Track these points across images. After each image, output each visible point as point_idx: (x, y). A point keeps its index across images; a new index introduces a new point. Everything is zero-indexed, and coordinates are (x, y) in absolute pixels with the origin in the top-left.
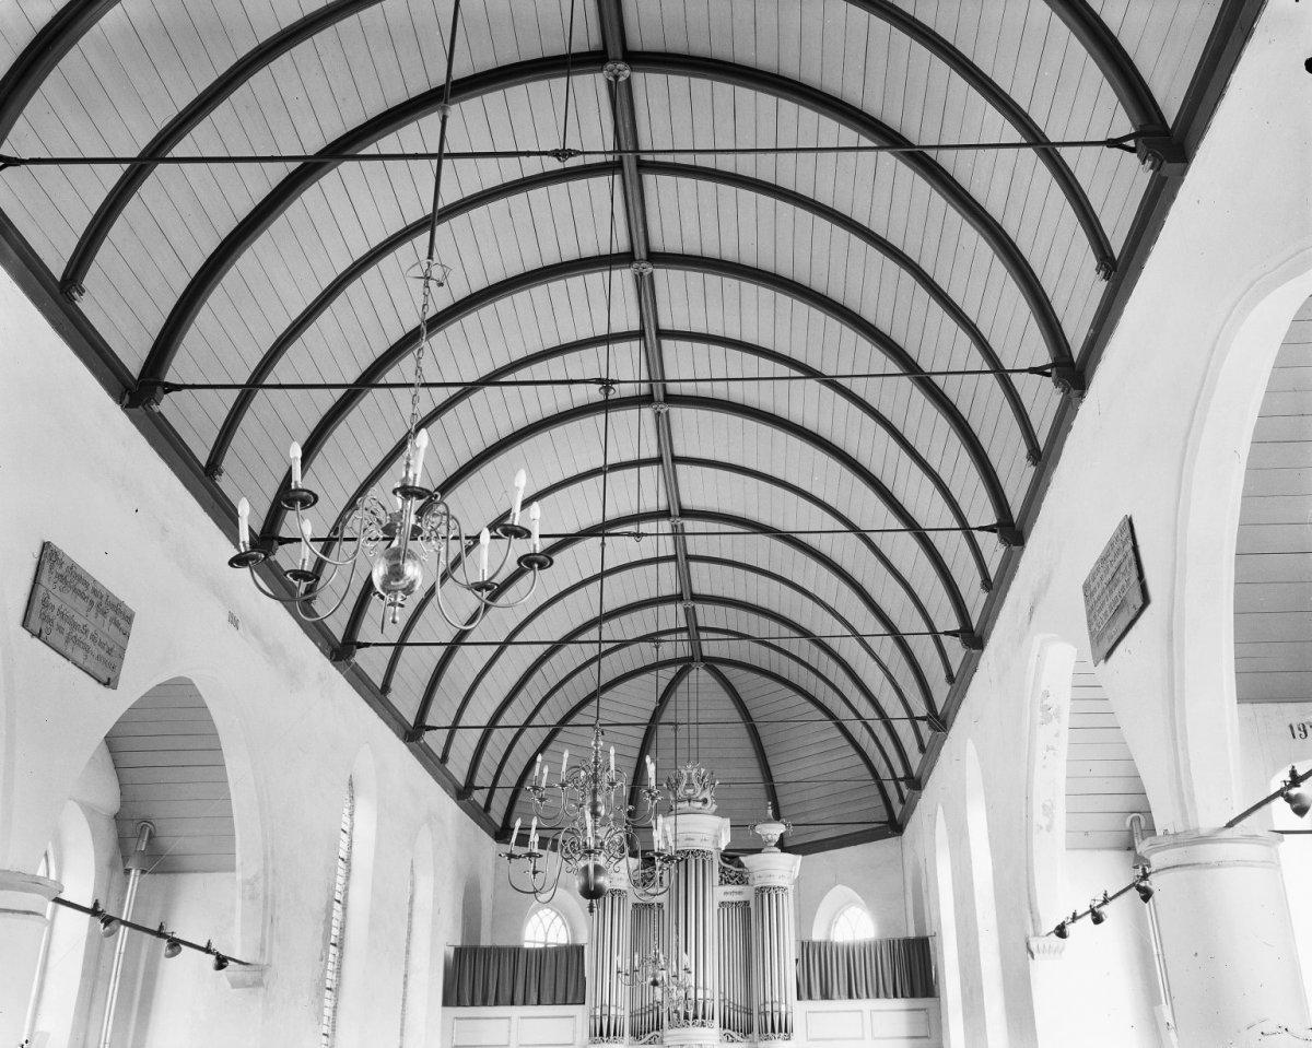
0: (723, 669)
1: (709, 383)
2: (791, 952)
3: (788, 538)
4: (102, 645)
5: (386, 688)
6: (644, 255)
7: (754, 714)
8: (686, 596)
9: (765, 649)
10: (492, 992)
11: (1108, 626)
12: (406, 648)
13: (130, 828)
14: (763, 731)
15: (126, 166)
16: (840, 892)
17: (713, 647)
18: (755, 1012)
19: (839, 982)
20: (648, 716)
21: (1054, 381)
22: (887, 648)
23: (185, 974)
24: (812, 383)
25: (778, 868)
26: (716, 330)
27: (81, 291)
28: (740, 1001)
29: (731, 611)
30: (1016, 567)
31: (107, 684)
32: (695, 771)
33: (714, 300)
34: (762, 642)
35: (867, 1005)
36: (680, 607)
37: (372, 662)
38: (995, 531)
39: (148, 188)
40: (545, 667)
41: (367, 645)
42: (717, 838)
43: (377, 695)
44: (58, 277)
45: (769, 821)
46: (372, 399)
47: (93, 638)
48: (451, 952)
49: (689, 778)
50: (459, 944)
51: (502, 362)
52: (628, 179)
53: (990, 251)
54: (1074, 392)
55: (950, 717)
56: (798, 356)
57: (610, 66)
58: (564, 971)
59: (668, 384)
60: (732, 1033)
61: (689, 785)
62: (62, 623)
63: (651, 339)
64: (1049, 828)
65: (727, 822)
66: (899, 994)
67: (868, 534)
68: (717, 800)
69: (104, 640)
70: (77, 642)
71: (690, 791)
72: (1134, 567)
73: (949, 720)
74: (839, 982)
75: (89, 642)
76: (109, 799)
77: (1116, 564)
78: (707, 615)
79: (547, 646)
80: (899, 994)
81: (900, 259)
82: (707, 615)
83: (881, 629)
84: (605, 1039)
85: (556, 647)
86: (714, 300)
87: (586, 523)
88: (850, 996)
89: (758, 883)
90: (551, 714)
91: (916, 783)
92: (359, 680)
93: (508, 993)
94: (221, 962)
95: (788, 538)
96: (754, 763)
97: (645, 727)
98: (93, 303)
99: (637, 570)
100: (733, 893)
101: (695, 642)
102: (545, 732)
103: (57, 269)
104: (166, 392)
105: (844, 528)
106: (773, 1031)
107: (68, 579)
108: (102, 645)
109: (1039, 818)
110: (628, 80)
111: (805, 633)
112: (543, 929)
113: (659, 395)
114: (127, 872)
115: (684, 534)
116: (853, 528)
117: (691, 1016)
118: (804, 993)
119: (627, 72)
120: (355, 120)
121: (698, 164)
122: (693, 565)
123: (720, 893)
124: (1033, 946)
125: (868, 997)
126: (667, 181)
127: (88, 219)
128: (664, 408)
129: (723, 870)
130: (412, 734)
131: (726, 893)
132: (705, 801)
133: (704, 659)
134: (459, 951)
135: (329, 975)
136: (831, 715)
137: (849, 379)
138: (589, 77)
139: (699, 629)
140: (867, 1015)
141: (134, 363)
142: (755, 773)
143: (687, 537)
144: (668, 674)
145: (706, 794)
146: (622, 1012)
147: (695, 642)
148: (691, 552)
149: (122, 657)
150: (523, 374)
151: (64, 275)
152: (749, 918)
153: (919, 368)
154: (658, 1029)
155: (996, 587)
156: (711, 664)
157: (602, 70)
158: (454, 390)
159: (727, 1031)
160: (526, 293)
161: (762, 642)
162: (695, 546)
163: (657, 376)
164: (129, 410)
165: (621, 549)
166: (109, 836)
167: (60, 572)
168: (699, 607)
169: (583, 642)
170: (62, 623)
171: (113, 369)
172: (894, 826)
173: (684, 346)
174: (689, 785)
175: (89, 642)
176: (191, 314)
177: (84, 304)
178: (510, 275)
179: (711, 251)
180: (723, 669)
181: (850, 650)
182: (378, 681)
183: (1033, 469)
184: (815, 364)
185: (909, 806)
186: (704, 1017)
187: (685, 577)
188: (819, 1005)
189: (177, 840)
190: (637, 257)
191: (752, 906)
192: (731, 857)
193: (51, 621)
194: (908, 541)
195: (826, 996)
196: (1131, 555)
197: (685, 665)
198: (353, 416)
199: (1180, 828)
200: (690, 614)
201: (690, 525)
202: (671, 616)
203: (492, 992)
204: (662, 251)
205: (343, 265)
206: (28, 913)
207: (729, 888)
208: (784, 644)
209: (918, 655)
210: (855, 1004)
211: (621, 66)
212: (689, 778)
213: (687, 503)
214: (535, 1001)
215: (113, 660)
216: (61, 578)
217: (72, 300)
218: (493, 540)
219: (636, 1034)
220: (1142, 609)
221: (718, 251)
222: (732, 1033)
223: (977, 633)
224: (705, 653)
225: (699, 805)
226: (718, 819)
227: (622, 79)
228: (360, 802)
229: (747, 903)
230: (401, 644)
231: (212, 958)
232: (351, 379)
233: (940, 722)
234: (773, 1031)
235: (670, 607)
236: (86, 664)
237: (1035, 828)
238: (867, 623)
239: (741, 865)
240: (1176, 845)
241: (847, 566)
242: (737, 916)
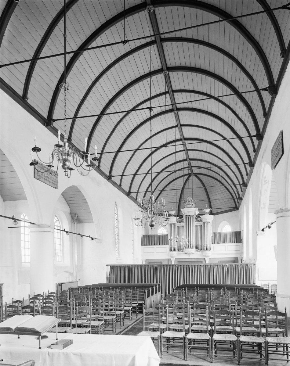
0: (198, 175)
1: (183, 104)
2: (211, 234)
3: (210, 143)
4: (52, 180)
5: (120, 185)
6: (166, 68)
7: (206, 185)
8: (188, 159)
9: (207, 170)
10: (150, 243)
11: (275, 160)
12: (121, 175)
13: (73, 215)
14: (208, 189)
15: (30, 62)
16: (224, 222)
17: (196, 171)
18: (203, 246)
19: (221, 240)
20: (182, 187)
21: (269, 92)
22: (234, 168)
23: (87, 240)
24: (212, 100)
25: (208, 218)
26: (187, 88)
27: (28, 99)
28: (200, 244)
29: (199, 162)
30: (261, 146)
31: (55, 188)
34: (207, 169)
35: (226, 245)
36: (187, 162)
37: (117, 180)
38: (255, 137)
39: (37, 68)
40: (157, 178)
41: (114, 176)
42: (195, 212)
43: (119, 187)
44: (22, 95)
45: (207, 208)
46: (104, 118)
47: (50, 179)
48: (142, 236)
49: (189, 200)
50: (144, 234)
51: (135, 105)
52: (158, 45)
53: (255, 53)
54: (274, 95)
55: (248, 183)
56: (209, 93)
57: (148, 7)
58: (164, 239)
59: (177, 105)
61: (189, 202)
62: (43, 176)
63: (171, 94)
64: (264, 208)
65: (197, 209)
66: (234, 242)
67: (229, 140)
68: (195, 204)
69: (53, 179)
70: (47, 180)
71: (189, 203)
72: (281, 144)
73: (247, 184)
74: (221, 240)
75: (49, 180)
76: (68, 210)
77: (278, 144)
78: (193, 163)
79: (157, 173)
80: (234, 242)
81: (110, 67)
82: (193, 163)
83: (233, 164)
85: (159, 173)
87: (162, 144)
88: (223, 243)
89: (204, 221)
90: (160, 188)
91: (241, 199)
92: (114, 184)
93: (154, 243)
94: (92, 239)
95: (210, 143)
96: (206, 196)
98: (31, 100)
99: (172, 155)
100: (199, 223)
101: (192, 170)
102: (159, 192)
103: (21, 94)
104: (54, 122)
105: (223, 139)
106: (206, 249)
107: (42, 167)
108: (52, 180)
109: (262, 206)
110: (154, 10)
111: (216, 166)
112: (161, 231)
113: (175, 109)
114: (74, 223)
115: (185, 144)
116: (225, 139)
117: (189, 247)
118: (213, 242)
119: (153, 8)
120: (84, 39)
121: (177, 37)
122: (188, 151)
124: (258, 233)
125: (233, 243)
126: (169, 44)
127: (25, 79)
128: (176, 112)
129: (196, 219)
130: (128, 194)
131: (182, 224)
132: (192, 205)
133: (194, 173)
134: (144, 236)
135: (116, 240)
136: (223, 184)
137: (222, 97)
138: (143, 12)
139: (192, 167)
141: (45, 115)
142: (206, 198)
143: (186, 145)
144: (186, 177)
145: (193, 203)
146: (176, 246)
147: (192, 170)
148: (188, 148)
149: (57, 182)
150: (140, 107)
151: (23, 95)
152: (202, 228)
153: (239, 92)
155: (256, 151)
156: (196, 175)
157: (146, 9)
158: (124, 113)
160: (142, 82)
161: (207, 169)
162: (189, 147)
163: (174, 103)
164: (47, 127)
165: (171, 149)
166: (70, 217)
167: (39, 165)
168: (191, 162)
169: (171, 171)
170: (43, 176)
171: (42, 119)
172: (237, 208)
173: (179, 94)
174: (189, 202)
175: (49, 180)
176: (55, 101)
177: (29, 101)
178: (133, 80)
179: (183, 65)
180: (198, 175)
181: (226, 169)
182: (119, 184)
183: (265, 119)
184: (213, 94)
185: (240, 204)
186: (192, 247)
187: (187, 155)
188: (216, 244)
189: (81, 217)
190: (164, 69)
191: (203, 226)
192: (198, 216)
193: (40, 176)
194: (237, 141)
195: (218, 243)
196: (281, 141)
197: (189, 175)
198: (101, 123)
199: (284, 208)
200: (190, 163)
201: (187, 142)
202: (186, 164)
203: (150, 243)
204: (170, 66)
205: (90, 83)
206: (49, 232)
208: (212, 169)
209: (225, 170)
210: (224, 244)
211: (151, 6)
212: (189, 200)
213: (186, 136)
214: (154, 244)
215: (56, 183)
216: (40, 167)
217: (26, 101)
218: (91, 155)
219: (179, 250)
220: (282, 155)
221: (185, 63)
223: (253, 163)
224: (194, 172)
225: (191, 206)
226: (195, 209)
227: (152, 11)
228: (119, 208)
229: (201, 225)
230: (122, 176)
231: (91, 239)
232: (99, 113)
233: (245, 185)
234: (206, 249)
235: (185, 162)
236: (50, 184)
237: (261, 208)
238: (230, 162)
239: (200, 218)
240: (282, 212)
241: (225, 149)
242: (199, 228)
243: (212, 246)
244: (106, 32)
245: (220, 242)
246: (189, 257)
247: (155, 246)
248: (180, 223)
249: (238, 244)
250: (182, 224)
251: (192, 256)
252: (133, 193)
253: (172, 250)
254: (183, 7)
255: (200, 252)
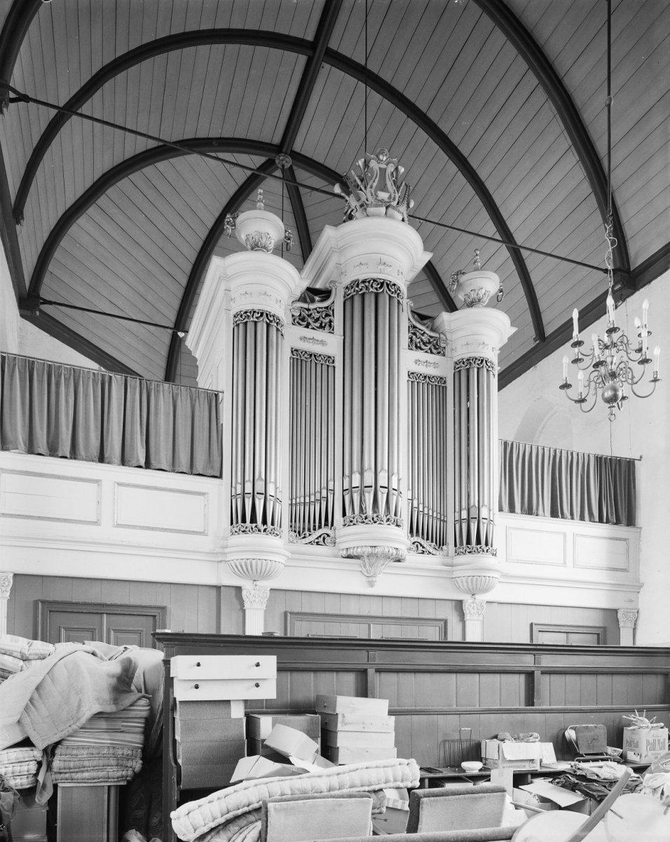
32: (391, 168)
33: (113, 211)
60: (423, 542)
84: (262, 528)
86: (113, 211)
89: (461, 353)
97: (249, 173)
123: (411, 361)
125: (582, 518)
126: (338, 74)
131: (323, 343)
140: (569, 538)
154: (326, 525)
159: (415, 539)
207: (420, 355)
210: (558, 523)
222: (423, 542)
242: (107, 455)
243: (506, 529)
244: (258, 48)
245: (540, 512)
246: (371, 584)
247: (112, 473)
248: (309, 333)
249: (622, 531)
250: (323, 343)
251: (389, 582)
252: (592, 537)
253: (248, 516)
254: (356, 80)
255: (434, 560)
